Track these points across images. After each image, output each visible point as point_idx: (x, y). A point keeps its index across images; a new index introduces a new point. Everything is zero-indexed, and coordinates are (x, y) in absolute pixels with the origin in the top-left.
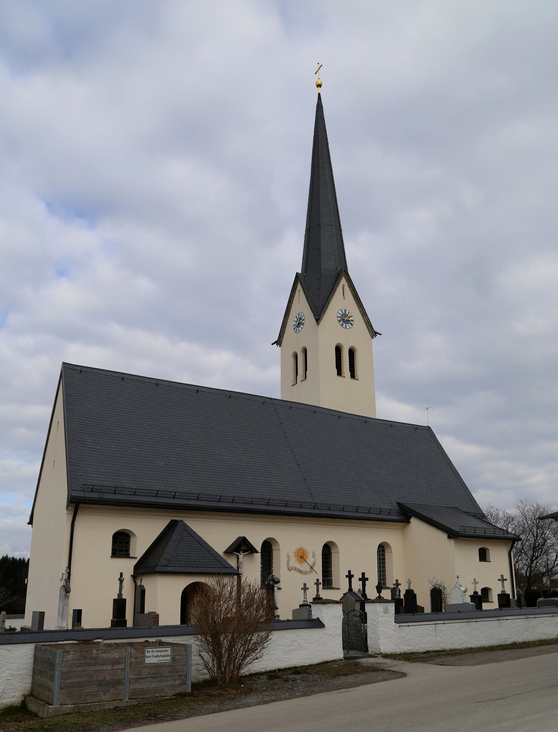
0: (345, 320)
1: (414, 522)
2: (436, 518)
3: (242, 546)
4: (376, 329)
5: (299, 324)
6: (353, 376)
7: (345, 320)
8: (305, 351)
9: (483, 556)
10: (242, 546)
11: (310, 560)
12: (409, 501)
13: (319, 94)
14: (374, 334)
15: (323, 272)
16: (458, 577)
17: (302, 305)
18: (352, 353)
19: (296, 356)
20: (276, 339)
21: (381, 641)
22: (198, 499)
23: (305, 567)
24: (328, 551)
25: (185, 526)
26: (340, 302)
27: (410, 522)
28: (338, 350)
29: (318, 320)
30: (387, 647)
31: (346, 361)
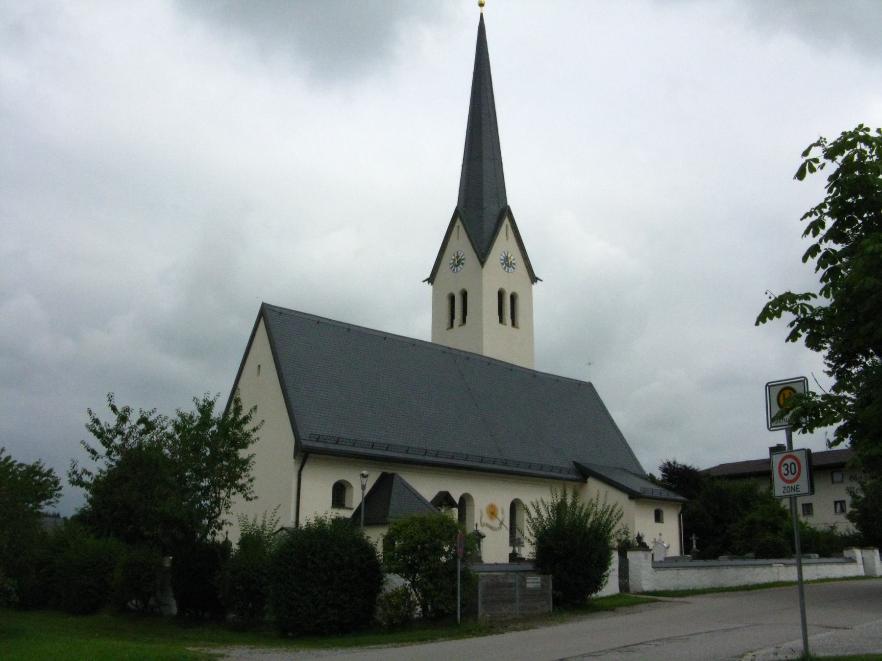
0: (507, 263)
1: (591, 482)
2: (616, 478)
3: (444, 499)
4: (537, 275)
5: (458, 262)
6: (514, 324)
7: (507, 263)
8: (464, 295)
9: (658, 518)
10: (444, 499)
11: (500, 516)
12: (586, 460)
13: (482, 15)
14: (534, 279)
15: (482, 208)
16: (660, 535)
17: (462, 244)
18: (513, 298)
19: (452, 298)
20: (428, 275)
21: (643, 582)
22: (354, 445)
23: (495, 523)
24: (514, 506)
25: (401, 479)
26: (503, 244)
27: (586, 482)
28: (501, 294)
29: (482, 263)
30: (647, 586)
31: (509, 308)
